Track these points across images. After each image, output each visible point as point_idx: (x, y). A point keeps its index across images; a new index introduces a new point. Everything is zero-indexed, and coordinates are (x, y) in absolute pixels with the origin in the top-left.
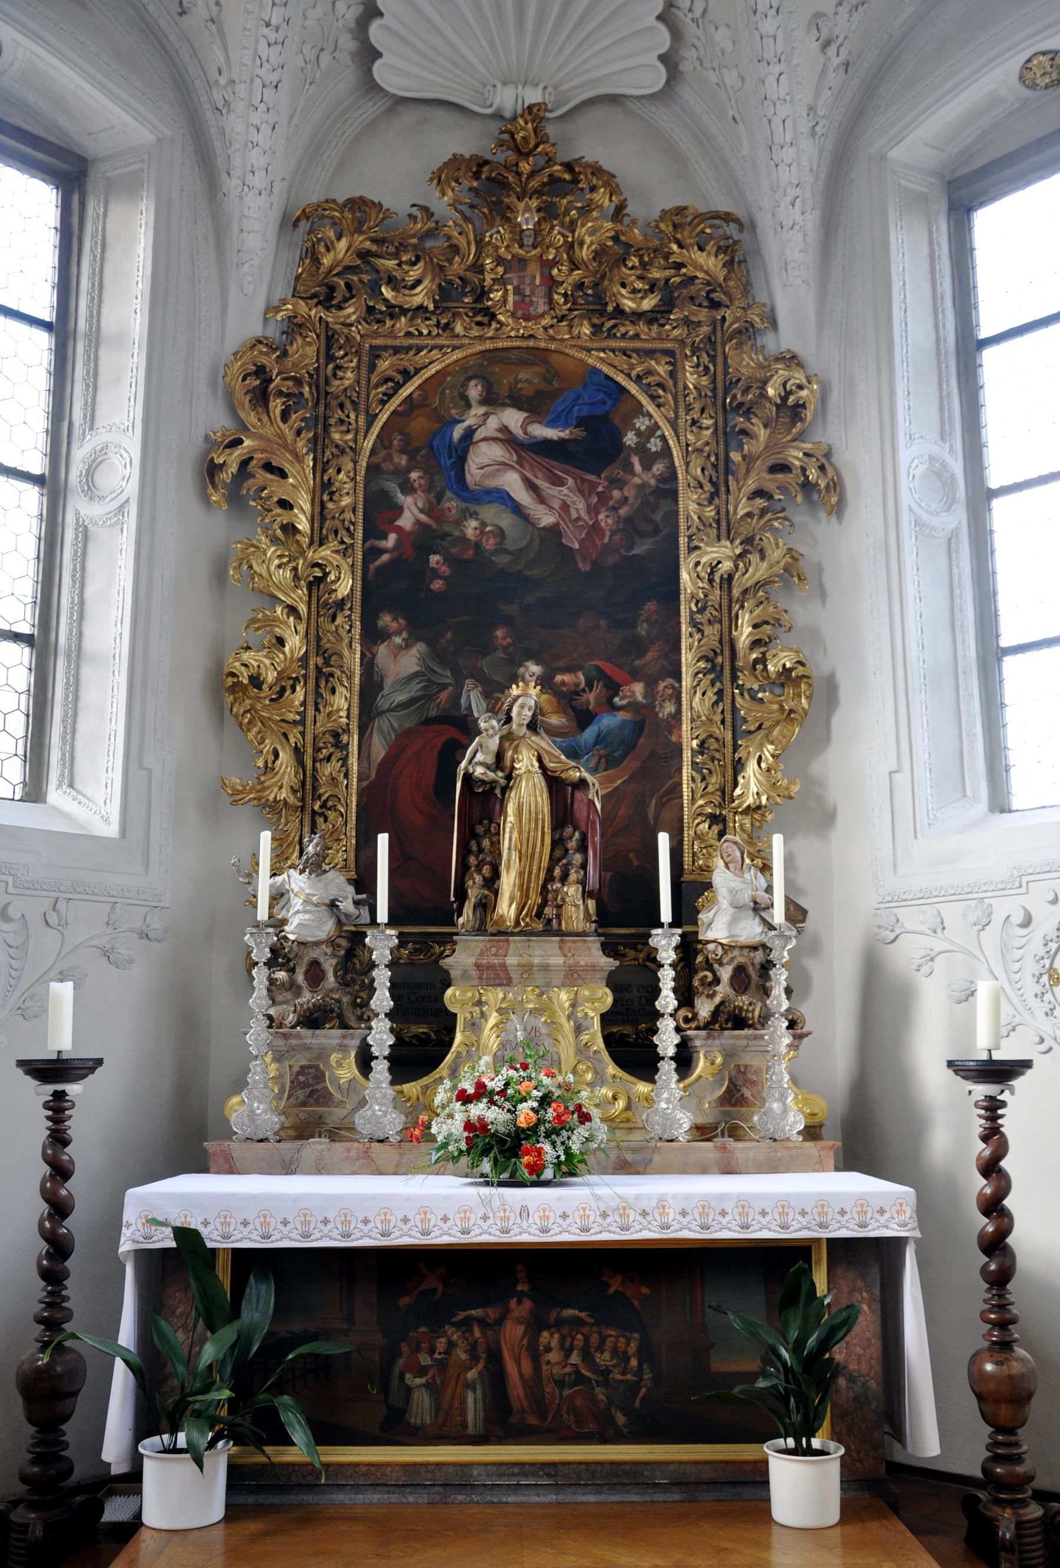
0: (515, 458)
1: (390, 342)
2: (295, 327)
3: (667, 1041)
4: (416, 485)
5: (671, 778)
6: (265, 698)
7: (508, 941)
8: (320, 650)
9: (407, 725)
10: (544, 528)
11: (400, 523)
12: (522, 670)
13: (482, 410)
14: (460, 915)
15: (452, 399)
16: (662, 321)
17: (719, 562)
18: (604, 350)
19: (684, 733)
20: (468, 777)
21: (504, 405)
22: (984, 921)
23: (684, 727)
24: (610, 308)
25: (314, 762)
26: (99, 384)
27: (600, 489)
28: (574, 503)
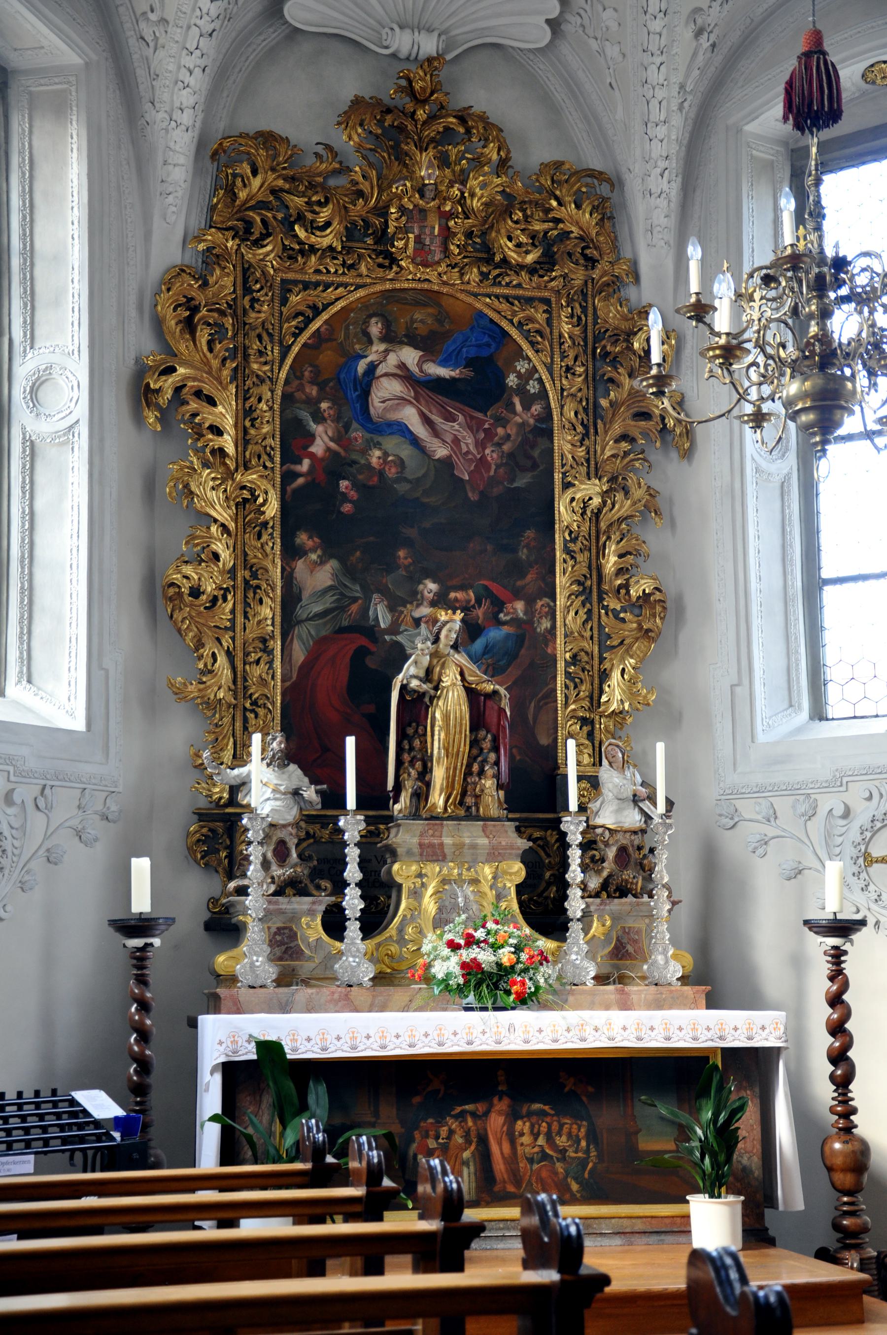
0: (412, 394)
1: (299, 277)
2: (213, 258)
3: (575, 904)
4: (326, 415)
5: (547, 685)
6: (200, 606)
8: (247, 565)
9: (324, 633)
10: (439, 459)
11: (313, 449)
12: (421, 587)
13: (382, 347)
14: (396, 801)
15: (356, 335)
16: (541, 272)
17: (590, 499)
18: (489, 296)
19: (558, 646)
21: (401, 343)
22: (811, 813)
23: (558, 642)
24: (497, 258)
25: (245, 664)
26: (37, 304)
27: (486, 426)
28: (464, 438)
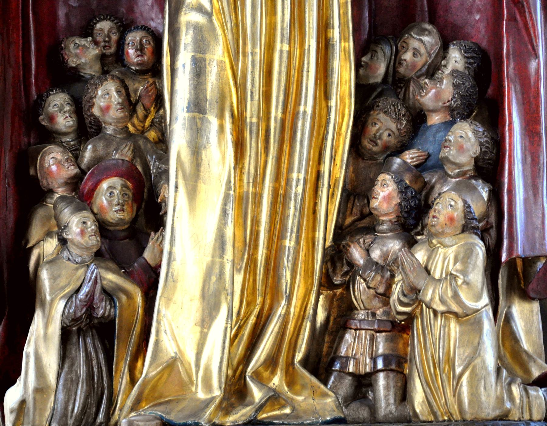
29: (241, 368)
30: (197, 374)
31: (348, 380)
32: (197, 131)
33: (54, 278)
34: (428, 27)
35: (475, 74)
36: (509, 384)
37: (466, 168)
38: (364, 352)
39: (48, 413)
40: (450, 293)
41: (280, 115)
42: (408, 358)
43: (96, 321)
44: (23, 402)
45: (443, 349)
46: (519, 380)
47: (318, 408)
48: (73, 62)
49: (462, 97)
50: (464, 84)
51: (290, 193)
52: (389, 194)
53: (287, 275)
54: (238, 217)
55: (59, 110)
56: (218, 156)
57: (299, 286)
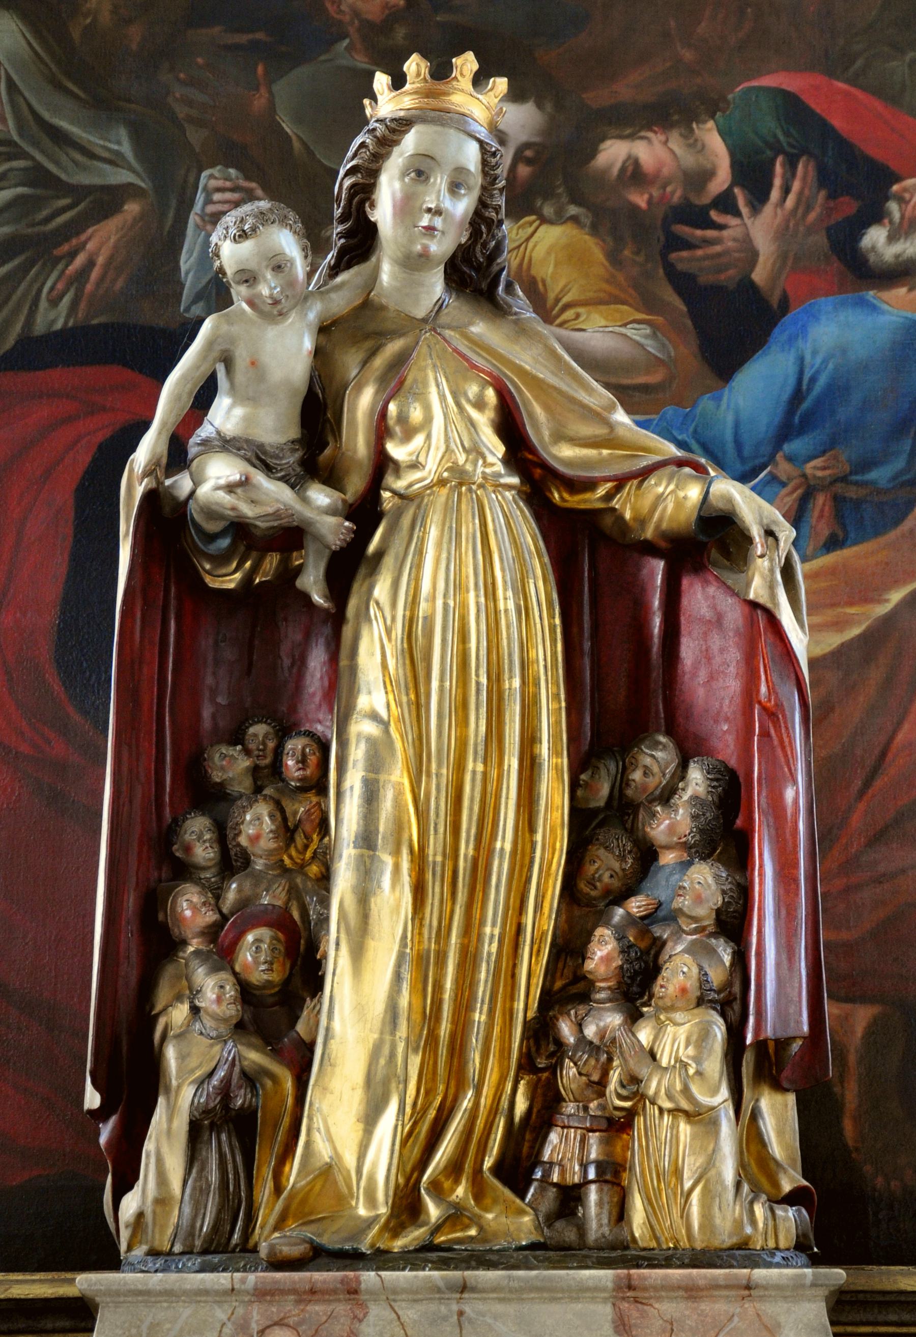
7: (353, 1291)
20: (165, 517)
29: (415, 1175)
30: (358, 1184)
31: (552, 1192)
32: (367, 873)
33: (182, 1057)
34: (662, 739)
35: (720, 800)
36: (751, 1203)
37: (706, 923)
38: (572, 1157)
39: (170, 1230)
40: (678, 1086)
41: (471, 852)
42: (628, 1166)
43: (233, 1113)
44: (140, 1215)
45: (670, 1157)
46: (764, 1197)
47: (512, 1228)
48: (217, 777)
49: (701, 831)
50: (704, 815)
51: (482, 952)
52: (608, 954)
53: (475, 1058)
54: (415, 982)
55: (198, 840)
56: (393, 900)
57: (492, 1069)
